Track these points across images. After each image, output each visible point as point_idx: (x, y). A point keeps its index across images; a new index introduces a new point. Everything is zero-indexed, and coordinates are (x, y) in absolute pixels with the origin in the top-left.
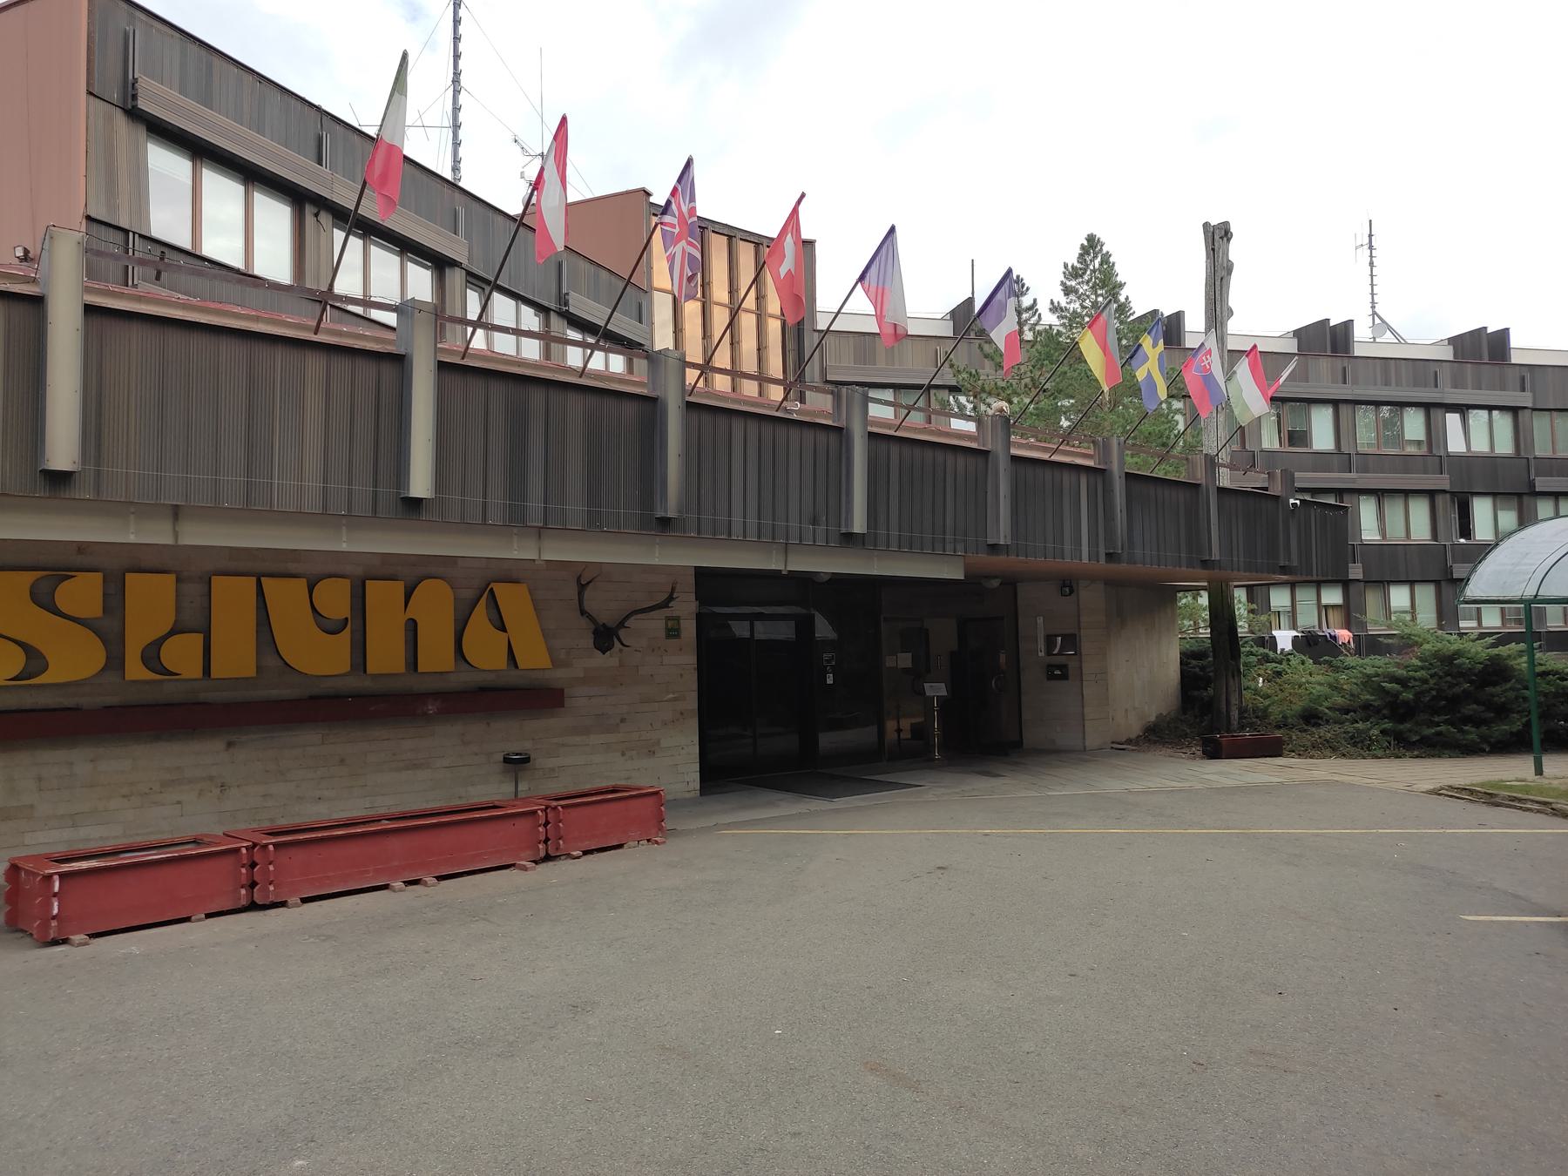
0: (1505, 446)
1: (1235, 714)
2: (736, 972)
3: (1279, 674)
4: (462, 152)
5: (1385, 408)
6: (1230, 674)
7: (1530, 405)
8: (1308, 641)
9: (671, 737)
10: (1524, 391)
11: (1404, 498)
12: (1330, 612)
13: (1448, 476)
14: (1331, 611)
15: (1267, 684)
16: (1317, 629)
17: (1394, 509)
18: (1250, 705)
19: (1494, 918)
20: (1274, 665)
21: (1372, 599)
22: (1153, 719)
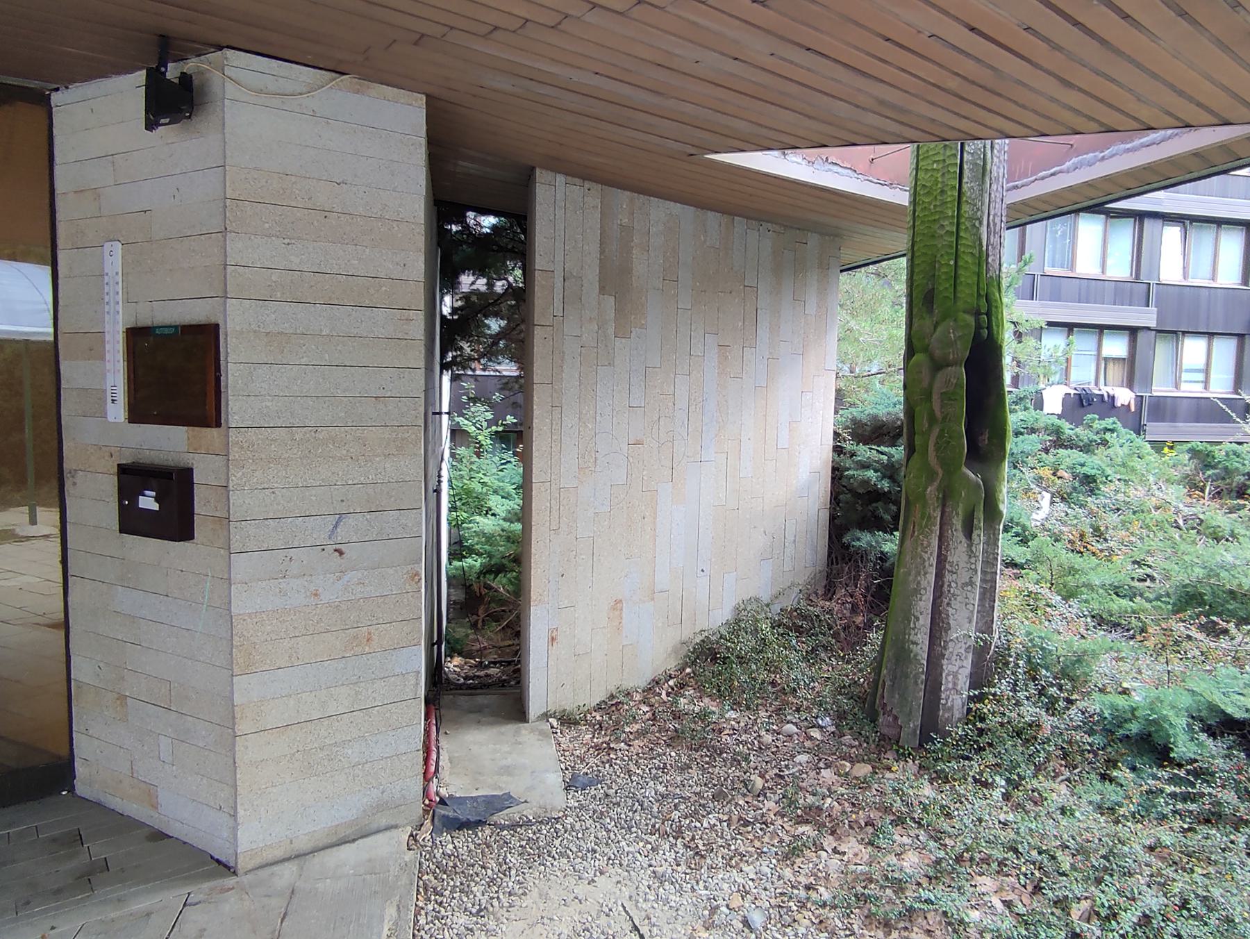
0: (483, 289)
2: (194, 788)
3: (1089, 483)
5: (976, 279)
6: (958, 523)
7: (1153, 324)
8: (1081, 401)
9: (1053, 425)
10: (1148, 306)
11: (1066, 335)
12: (1110, 366)
13: (1156, 309)
14: (1111, 364)
16: (1092, 386)
17: (1203, 238)
21: (1162, 351)
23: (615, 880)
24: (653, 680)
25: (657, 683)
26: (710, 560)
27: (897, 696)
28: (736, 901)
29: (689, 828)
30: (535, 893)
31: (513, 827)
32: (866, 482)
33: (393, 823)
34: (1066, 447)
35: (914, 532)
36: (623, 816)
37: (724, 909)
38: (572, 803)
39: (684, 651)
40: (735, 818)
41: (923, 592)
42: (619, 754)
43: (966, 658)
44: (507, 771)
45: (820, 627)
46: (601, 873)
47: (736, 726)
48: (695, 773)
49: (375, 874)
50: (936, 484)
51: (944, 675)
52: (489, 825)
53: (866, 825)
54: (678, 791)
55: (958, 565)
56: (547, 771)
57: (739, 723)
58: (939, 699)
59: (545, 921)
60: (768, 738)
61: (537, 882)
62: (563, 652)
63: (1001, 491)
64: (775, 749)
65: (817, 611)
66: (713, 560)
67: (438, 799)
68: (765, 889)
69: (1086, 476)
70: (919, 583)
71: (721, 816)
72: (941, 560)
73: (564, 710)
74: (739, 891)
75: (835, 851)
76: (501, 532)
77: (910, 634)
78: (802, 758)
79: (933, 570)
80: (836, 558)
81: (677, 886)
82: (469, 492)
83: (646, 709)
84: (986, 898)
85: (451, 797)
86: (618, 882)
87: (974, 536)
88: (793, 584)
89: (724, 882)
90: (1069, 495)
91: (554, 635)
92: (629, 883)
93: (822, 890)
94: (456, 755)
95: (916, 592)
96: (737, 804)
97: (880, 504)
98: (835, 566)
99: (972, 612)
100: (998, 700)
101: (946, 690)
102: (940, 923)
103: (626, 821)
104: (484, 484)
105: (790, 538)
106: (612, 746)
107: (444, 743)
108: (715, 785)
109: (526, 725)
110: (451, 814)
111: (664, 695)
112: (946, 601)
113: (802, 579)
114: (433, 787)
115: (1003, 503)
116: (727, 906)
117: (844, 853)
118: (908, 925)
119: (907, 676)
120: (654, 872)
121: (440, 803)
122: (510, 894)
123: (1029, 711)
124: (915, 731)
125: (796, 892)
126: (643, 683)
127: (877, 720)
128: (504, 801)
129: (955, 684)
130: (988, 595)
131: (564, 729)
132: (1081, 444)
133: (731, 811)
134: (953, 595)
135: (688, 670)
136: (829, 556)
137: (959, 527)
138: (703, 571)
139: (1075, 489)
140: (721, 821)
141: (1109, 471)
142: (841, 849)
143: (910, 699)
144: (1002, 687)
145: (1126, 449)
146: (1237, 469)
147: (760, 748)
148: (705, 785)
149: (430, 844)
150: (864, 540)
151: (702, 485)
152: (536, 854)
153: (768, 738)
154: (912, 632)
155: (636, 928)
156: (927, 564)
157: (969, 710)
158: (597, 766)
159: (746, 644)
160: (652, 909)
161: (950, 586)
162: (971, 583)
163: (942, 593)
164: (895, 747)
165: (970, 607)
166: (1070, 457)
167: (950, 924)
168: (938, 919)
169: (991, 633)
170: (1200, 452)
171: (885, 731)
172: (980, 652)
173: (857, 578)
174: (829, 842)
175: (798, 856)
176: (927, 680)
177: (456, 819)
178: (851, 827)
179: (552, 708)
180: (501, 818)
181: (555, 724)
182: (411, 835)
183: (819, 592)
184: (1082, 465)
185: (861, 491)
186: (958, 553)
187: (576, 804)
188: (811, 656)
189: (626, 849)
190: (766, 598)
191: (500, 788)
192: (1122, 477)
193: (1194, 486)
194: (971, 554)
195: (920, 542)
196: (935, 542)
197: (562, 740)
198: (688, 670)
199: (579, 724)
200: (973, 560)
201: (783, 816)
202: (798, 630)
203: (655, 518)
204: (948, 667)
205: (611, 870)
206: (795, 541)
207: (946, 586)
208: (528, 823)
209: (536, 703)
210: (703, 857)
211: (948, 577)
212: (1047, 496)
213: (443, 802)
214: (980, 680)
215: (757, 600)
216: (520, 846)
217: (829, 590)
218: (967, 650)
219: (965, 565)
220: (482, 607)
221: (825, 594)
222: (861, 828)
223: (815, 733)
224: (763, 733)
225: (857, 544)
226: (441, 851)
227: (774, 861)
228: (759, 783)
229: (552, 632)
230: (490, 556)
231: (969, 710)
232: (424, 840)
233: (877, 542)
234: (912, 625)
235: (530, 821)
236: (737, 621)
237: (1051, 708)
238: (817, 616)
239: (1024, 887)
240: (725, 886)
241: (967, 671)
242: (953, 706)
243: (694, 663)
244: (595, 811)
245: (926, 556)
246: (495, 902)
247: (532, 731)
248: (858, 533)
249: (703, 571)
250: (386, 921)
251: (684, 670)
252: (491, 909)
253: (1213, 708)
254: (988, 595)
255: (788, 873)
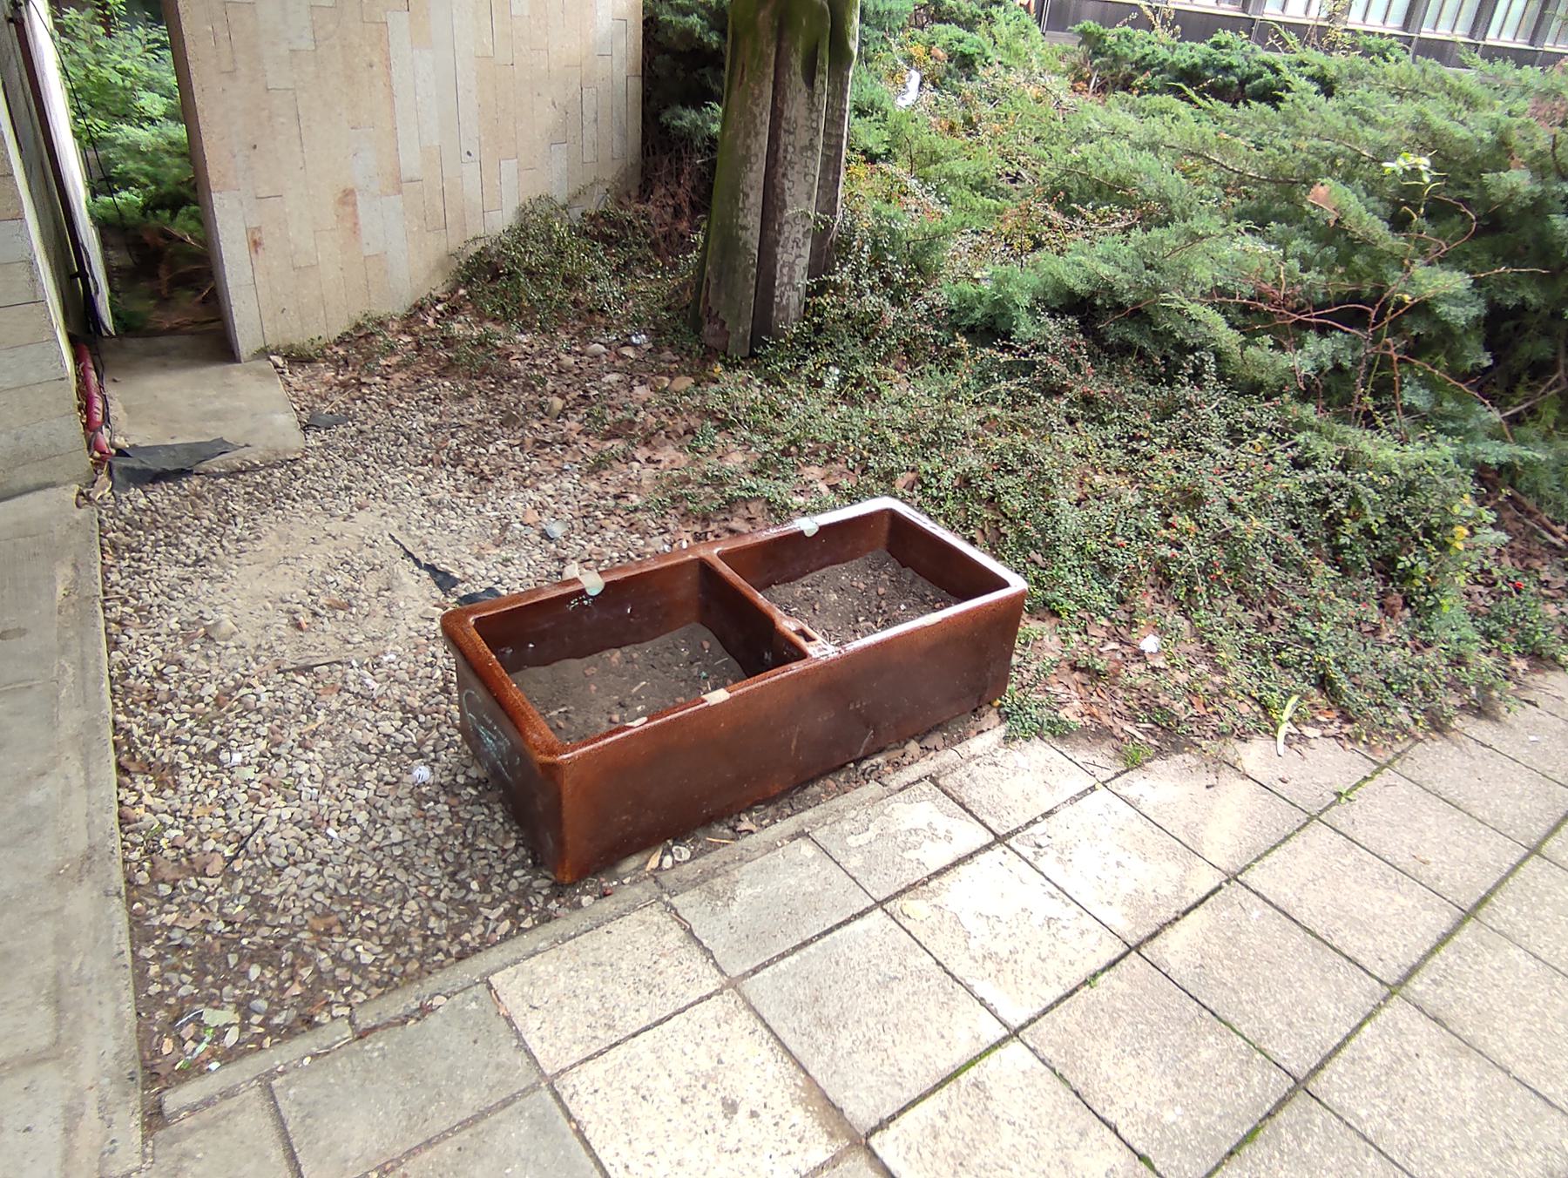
1: (795, 260)
3: (965, 63)
4: (1000, 1014)
6: (796, 63)
15: (930, 95)
18: (866, 223)
19: (680, 714)
20: (954, 31)
22: (501, 220)
23: (378, 513)
24: (415, 306)
25: (421, 309)
26: (479, 138)
27: (723, 296)
28: (532, 517)
29: (471, 454)
30: (273, 536)
31: (233, 473)
32: (688, 33)
33: (48, 480)
34: (945, 22)
35: (742, 78)
36: (385, 451)
37: (518, 526)
38: (313, 442)
39: (454, 265)
40: (528, 441)
41: (753, 160)
42: (373, 388)
43: (804, 244)
44: (218, 416)
45: (634, 236)
46: (360, 508)
47: (529, 350)
48: (477, 402)
49: (31, 536)
50: (770, 6)
51: (778, 267)
52: (198, 474)
53: (685, 433)
54: (455, 420)
55: (795, 122)
56: (273, 412)
57: (532, 346)
58: (773, 296)
59: (290, 561)
60: (570, 360)
61: (273, 526)
62: (275, 263)
63: (852, 22)
64: (578, 371)
65: (629, 215)
66: (483, 139)
67: (114, 451)
68: (567, 503)
69: (964, 56)
70: (748, 147)
71: (511, 442)
72: (777, 115)
73: (292, 346)
74: (535, 508)
75: (649, 460)
76: (168, 147)
77: (738, 217)
78: (613, 377)
79: (765, 131)
80: (653, 147)
81: (459, 511)
82: (105, 86)
83: (408, 339)
84: (812, 486)
85: (134, 447)
86: (383, 515)
87: (817, 83)
88: (597, 181)
89: (517, 503)
90: (942, 80)
91: (257, 237)
92: (396, 514)
93: (633, 497)
94: (134, 404)
95: (746, 160)
96: (531, 428)
97: (708, 71)
98: (652, 157)
99: (812, 185)
100: (837, 288)
101: (780, 285)
102: (763, 510)
103: (388, 456)
104: (125, 73)
105: (589, 115)
106: (363, 380)
107: (110, 390)
108: (502, 412)
109: (237, 365)
110: (137, 465)
111: (430, 321)
112: (781, 171)
113: (609, 175)
114: (104, 437)
115: (854, 39)
116: (521, 523)
117: (659, 461)
118: (728, 516)
119: (735, 271)
120: (428, 500)
121: (117, 455)
122: (238, 540)
123: (871, 301)
124: (745, 337)
125: (603, 502)
126: (402, 312)
127: (701, 329)
128: (220, 447)
129: (791, 278)
130: (832, 164)
131: (295, 368)
132: (963, 19)
133: (523, 435)
134: (790, 162)
135: (462, 292)
136: (644, 143)
137: (798, 69)
138: (469, 153)
139: (949, 72)
140: (511, 446)
141: (989, 52)
142: (656, 458)
143: (739, 298)
144: (843, 276)
145: (1012, 27)
146: (1126, 55)
147: (560, 372)
148: (491, 412)
149: (112, 501)
150: (687, 118)
151: (456, 21)
152: (269, 499)
153: (570, 360)
154: (741, 214)
155: (409, 554)
156: (758, 121)
157: (807, 304)
158: (345, 403)
159: (537, 255)
160: (429, 536)
161: (786, 151)
162: (812, 146)
163: (776, 160)
164: (721, 357)
165: (810, 178)
166: (950, 31)
167: (773, 510)
168: (760, 507)
169: (833, 213)
170: (1091, 34)
171: (711, 341)
172: (820, 237)
173: (679, 173)
174: (642, 453)
175: (606, 469)
176: (758, 272)
177: (145, 470)
178: (668, 437)
179: (272, 342)
180: (215, 465)
181: (280, 362)
182: (81, 493)
183: (633, 194)
184: (960, 41)
185: (682, 48)
186: (796, 108)
187: (320, 444)
188: (621, 270)
189: (391, 481)
190: (561, 199)
191: (207, 434)
192: (1004, 60)
193: (1078, 78)
194: (812, 107)
195: (749, 91)
196: (769, 92)
197: (293, 380)
198: (462, 292)
199: (315, 361)
200: (814, 116)
201: (587, 435)
202: (608, 240)
203: (389, 67)
204: (783, 256)
205: (373, 504)
206: (596, 120)
207: (781, 151)
208: (254, 469)
209: (246, 341)
210: (489, 480)
211: (784, 139)
212: (915, 77)
213: (121, 453)
214: (820, 265)
215: (549, 199)
216: (246, 493)
217: (645, 191)
218: (805, 234)
219: (804, 122)
220: (163, 266)
221: (640, 196)
222: (679, 437)
223: (629, 352)
224: (562, 356)
225: (677, 123)
226: (129, 506)
227: (577, 476)
228: (558, 403)
229: (253, 233)
230: (155, 180)
231: (807, 304)
232: (101, 497)
233: (704, 121)
234: (741, 205)
235: (256, 465)
236: (524, 228)
237: (896, 301)
238: (630, 222)
239: (853, 471)
240: (519, 505)
241: (805, 261)
242: (788, 304)
243: (469, 282)
244: (345, 449)
245: (756, 111)
246: (219, 551)
247: (248, 371)
248: (679, 110)
249: (469, 153)
250: (59, 581)
251: (456, 292)
252: (213, 558)
253: (1058, 285)
254: (832, 164)
255: (594, 486)
